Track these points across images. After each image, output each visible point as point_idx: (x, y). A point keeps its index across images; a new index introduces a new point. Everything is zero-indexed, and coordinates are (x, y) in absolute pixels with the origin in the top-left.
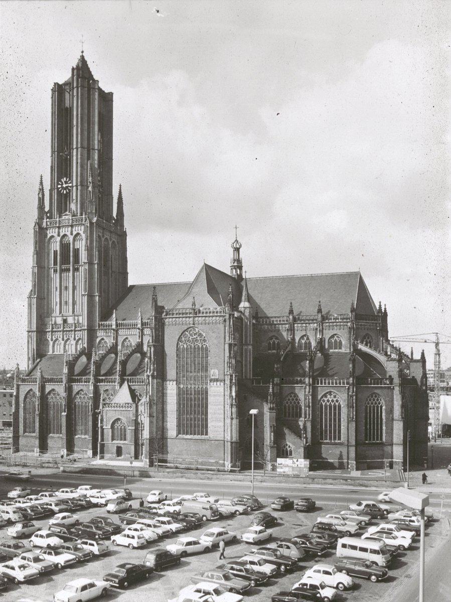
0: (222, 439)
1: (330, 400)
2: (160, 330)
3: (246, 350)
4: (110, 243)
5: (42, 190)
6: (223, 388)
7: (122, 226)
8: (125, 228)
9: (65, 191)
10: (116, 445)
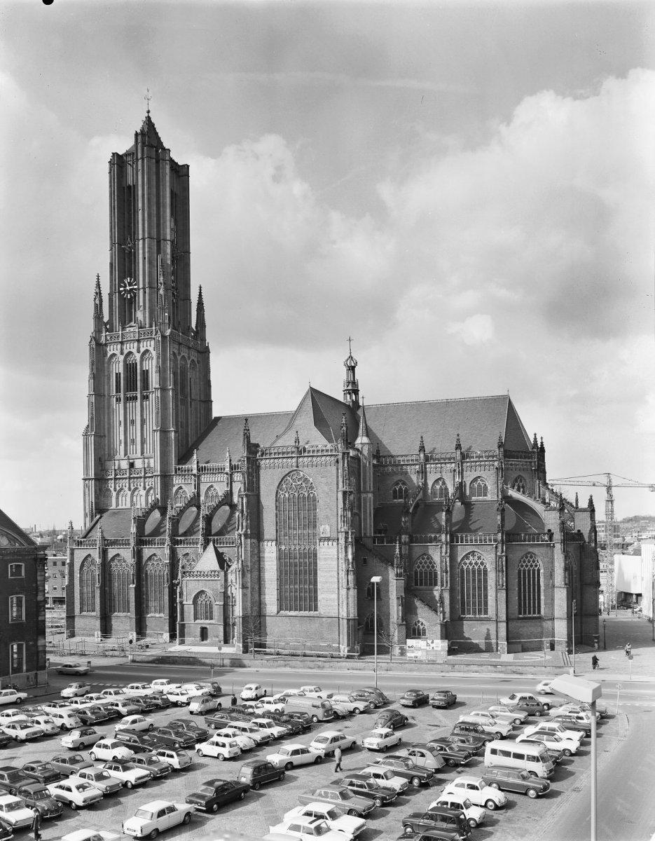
0: (337, 615)
1: (473, 562)
4: (189, 362)
7: (204, 340)
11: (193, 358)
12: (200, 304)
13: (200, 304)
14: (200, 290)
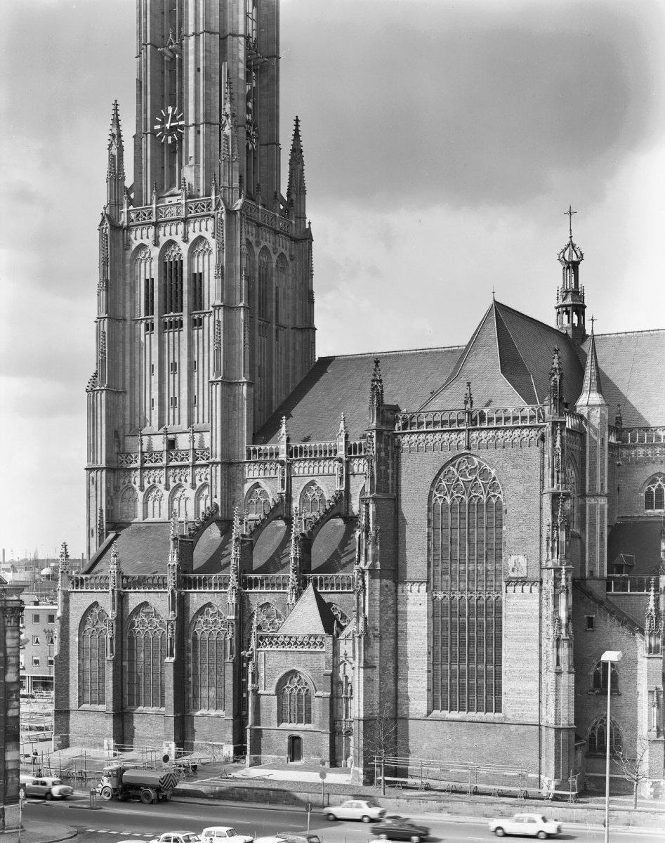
2: (390, 462)
3: (593, 508)
4: (274, 258)
5: (117, 137)
6: (538, 601)
7: (302, 217)
8: (307, 221)
9: (170, 138)
10: (287, 734)
11: (283, 251)
12: (297, 152)
13: (297, 152)
14: (297, 126)
